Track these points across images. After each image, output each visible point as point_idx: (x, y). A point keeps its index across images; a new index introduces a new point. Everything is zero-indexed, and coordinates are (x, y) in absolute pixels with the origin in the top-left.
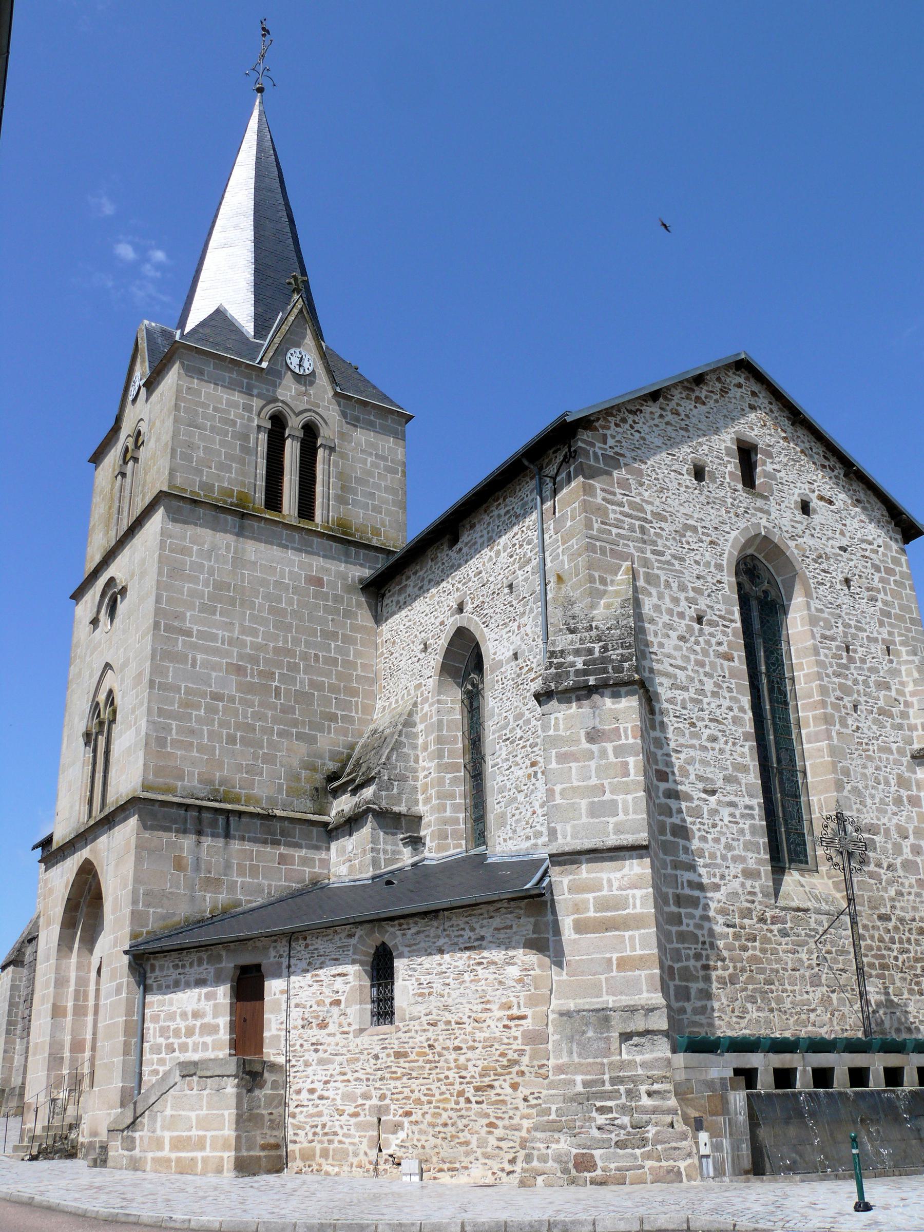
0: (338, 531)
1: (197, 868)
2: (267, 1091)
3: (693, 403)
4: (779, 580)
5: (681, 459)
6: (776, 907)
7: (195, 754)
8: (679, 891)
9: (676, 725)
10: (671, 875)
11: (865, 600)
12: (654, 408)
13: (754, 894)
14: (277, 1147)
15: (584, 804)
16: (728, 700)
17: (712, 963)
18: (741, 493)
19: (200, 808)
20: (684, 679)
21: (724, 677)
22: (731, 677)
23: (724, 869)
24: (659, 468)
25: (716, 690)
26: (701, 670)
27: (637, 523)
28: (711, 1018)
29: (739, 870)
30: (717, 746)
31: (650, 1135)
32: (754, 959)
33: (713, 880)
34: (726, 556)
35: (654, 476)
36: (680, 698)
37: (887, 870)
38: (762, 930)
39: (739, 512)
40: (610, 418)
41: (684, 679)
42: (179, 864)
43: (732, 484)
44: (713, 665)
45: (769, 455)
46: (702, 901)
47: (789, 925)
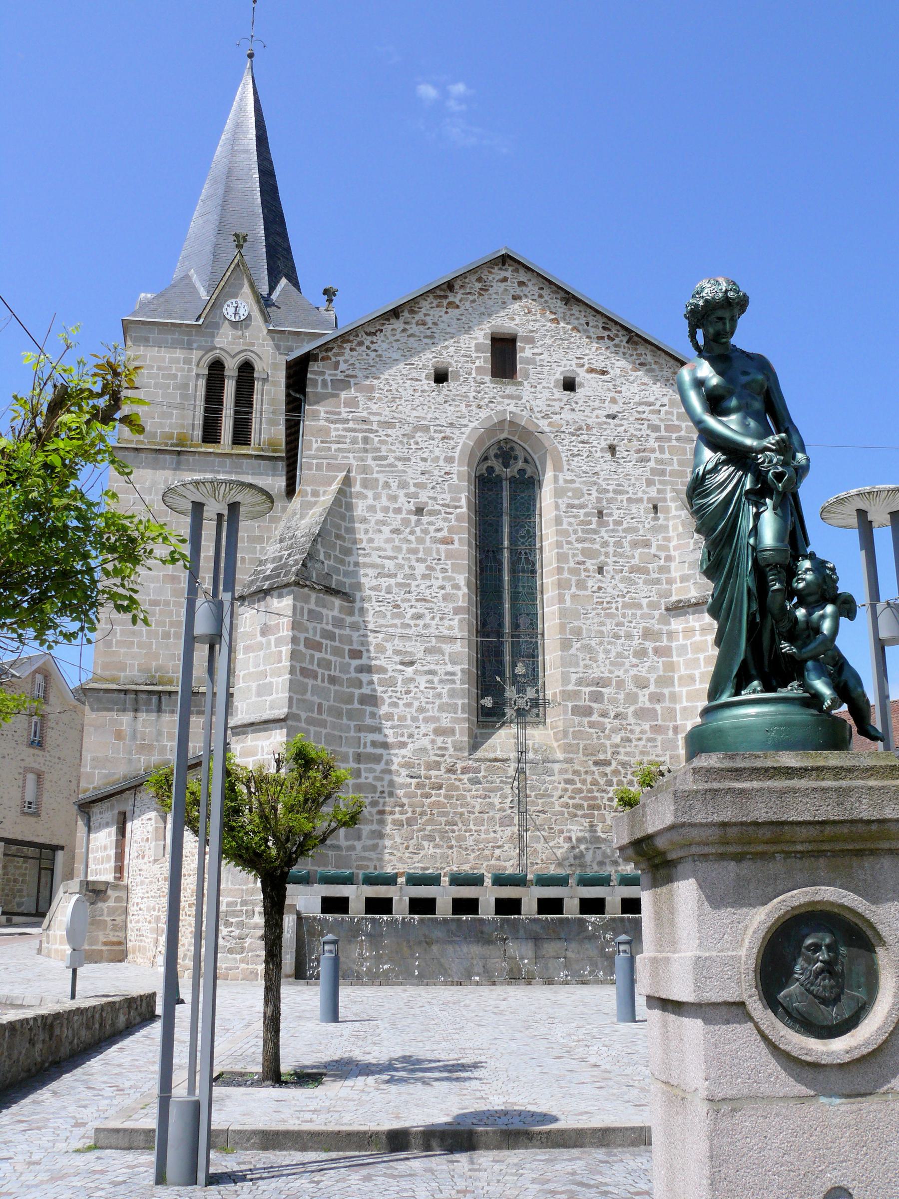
0: (267, 451)
1: (134, 737)
2: (111, 903)
3: (445, 309)
4: (535, 457)
5: (421, 366)
6: (470, 759)
7: (136, 650)
8: (361, 750)
9: (378, 609)
10: (353, 737)
11: (633, 463)
12: (398, 324)
13: (446, 749)
14: (120, 943)
15: (254, 686)
16: (440, 580)
17: (388, 809)
18: (489, 384)
19: (136, 692)
20: (392, 568)
21: (439, 559)
22: (447, 558)
23: (413, 729)
24: (394, 380)
25: (427, 572)
26: (413, 557)
27: (360, 435)
28: (382, 853)
29: (431, 730)
30: (421, 622)
31: (246, 945)
32: (437, 804)
33: (400, 739)
34: (459, 448)
35: (387, 387)
36: (384, 585)
37: (614, 719)
38: (450, 779)
39: (482, 403)
40: (345, 345)
41: (392, 568)
42: (119, 735)
43: (478, 378)
44: (428, 551)
45: (531, 340)
46: (385, 758)
47: (483, 773)
